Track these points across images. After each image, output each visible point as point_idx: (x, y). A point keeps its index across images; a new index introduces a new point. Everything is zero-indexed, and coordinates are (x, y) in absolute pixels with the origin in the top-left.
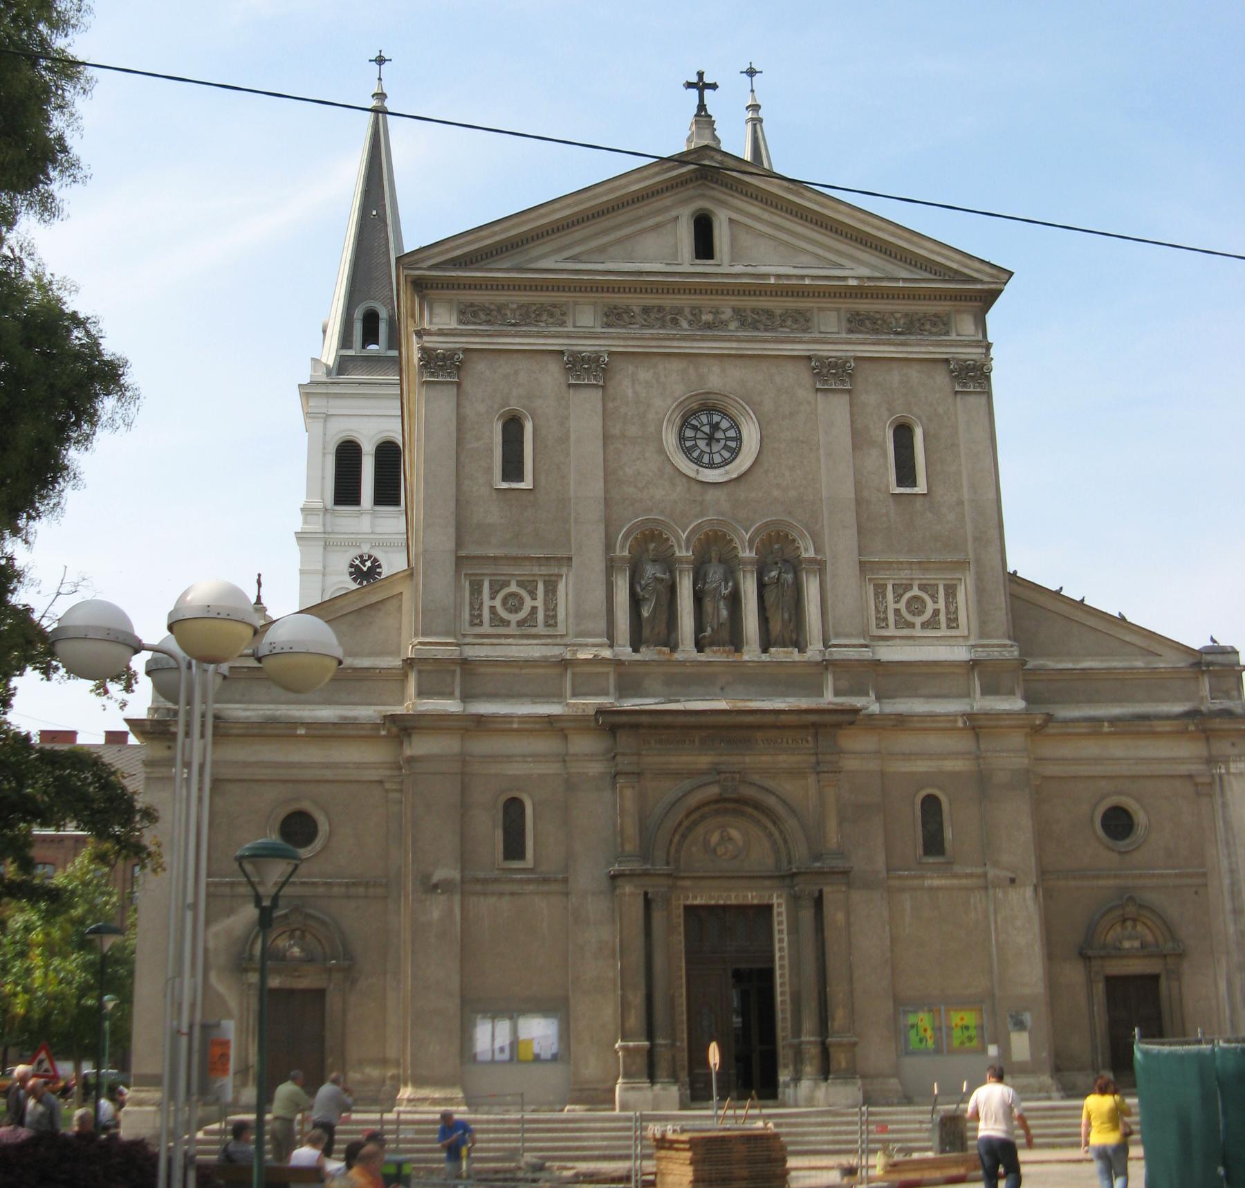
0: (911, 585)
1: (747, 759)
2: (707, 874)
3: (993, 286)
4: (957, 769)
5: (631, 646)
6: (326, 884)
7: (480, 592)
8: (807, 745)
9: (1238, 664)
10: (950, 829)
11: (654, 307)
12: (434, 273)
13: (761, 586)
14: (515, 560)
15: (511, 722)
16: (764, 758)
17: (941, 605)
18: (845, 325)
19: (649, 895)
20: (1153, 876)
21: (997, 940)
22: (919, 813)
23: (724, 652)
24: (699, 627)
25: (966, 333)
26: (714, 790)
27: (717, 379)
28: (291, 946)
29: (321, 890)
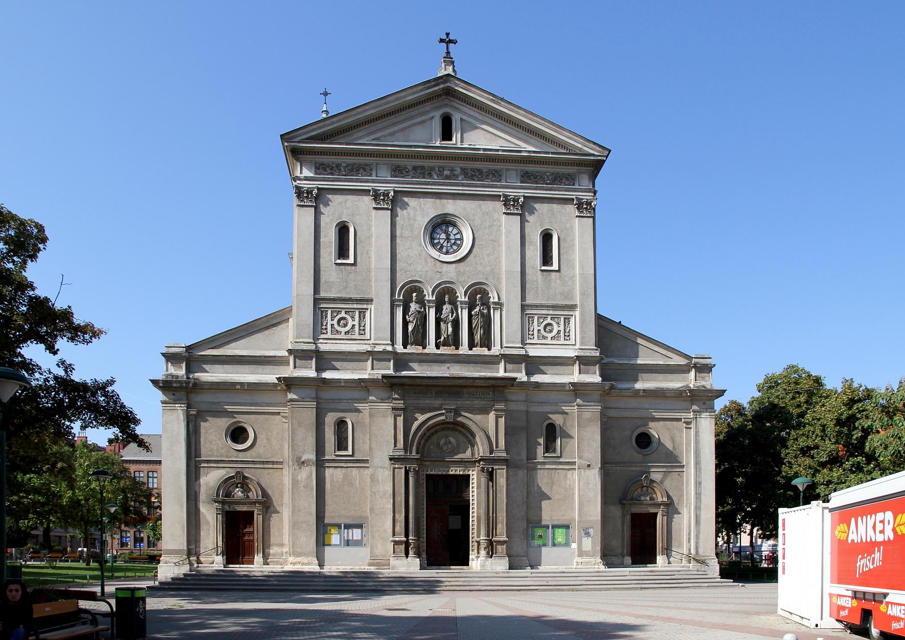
11: (419, 166)
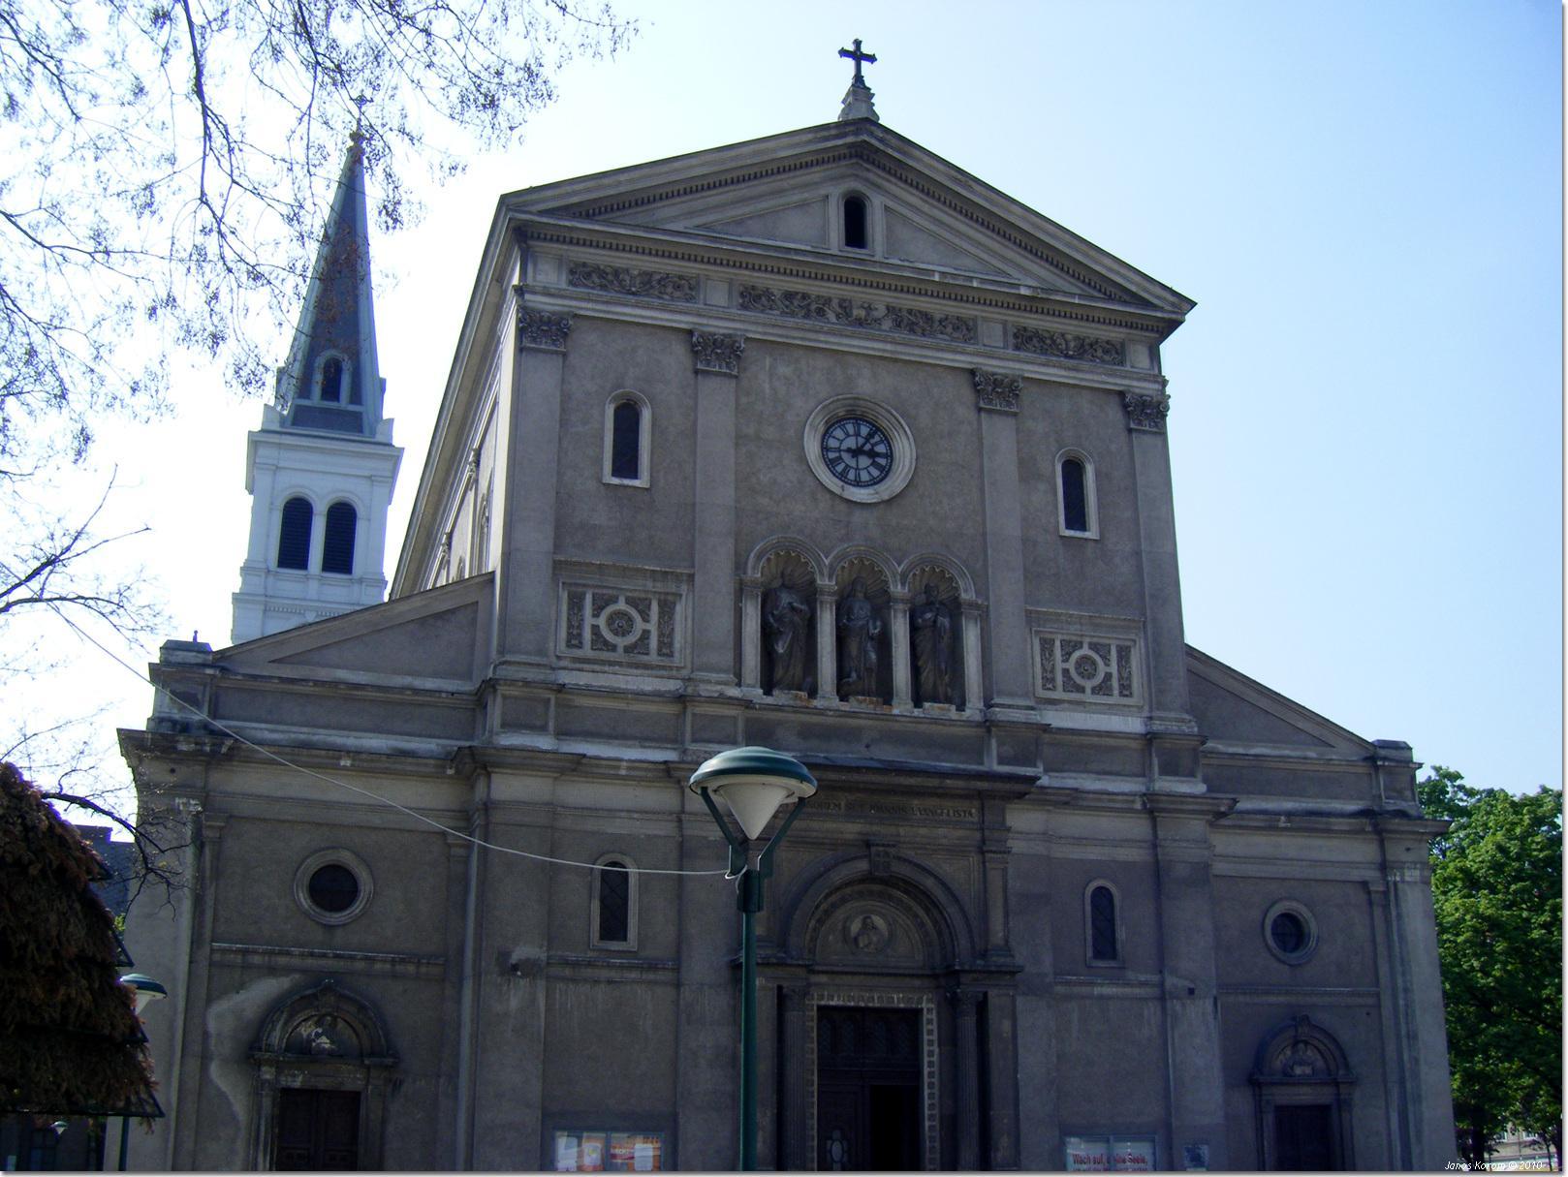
0: (1081, 643)
1: (902, 831)
2: (846, 969)
3: (1174, 316)
4: (1130, 859)
6: (367, 958)
7: (581, 608)
8: (971, 819)
9: (1412, 761)
11: (797, 293)
12: (544, 220)
13: (914, 629)
14: (625, 572)
15: (619, 768)
17: (1114, 669)
18: (1011, 340)
19: (785, 990)
20: (1326, 993)
21: (1174, 1061)
22: (1088, 908)
23: (871, 702)
24: (841, 674)
25: (1140, 366)
26: (863, 866)
27: (867, 385)
28: (318, 1035)
29: (360, 965)
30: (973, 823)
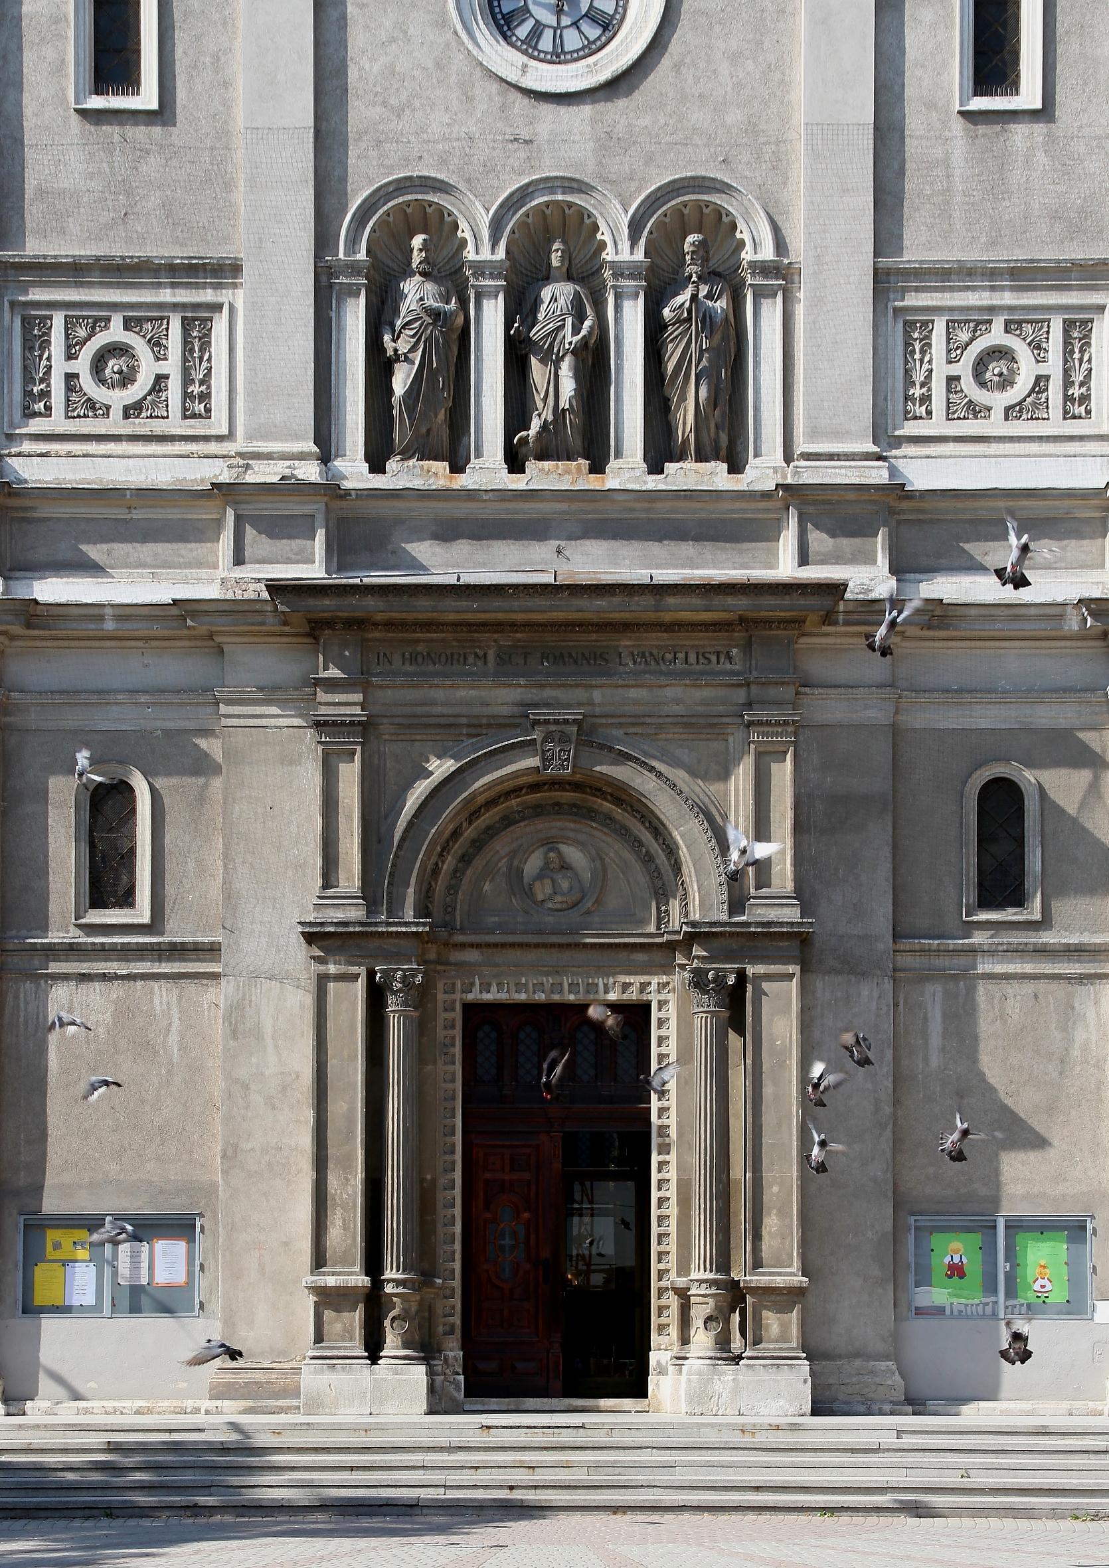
1: (597, 695)
5: (367, 459)
8: (728, 666)
10: (1039, 851)
16: (633, 693)
22: (973, 818)
30: (733, 673)
